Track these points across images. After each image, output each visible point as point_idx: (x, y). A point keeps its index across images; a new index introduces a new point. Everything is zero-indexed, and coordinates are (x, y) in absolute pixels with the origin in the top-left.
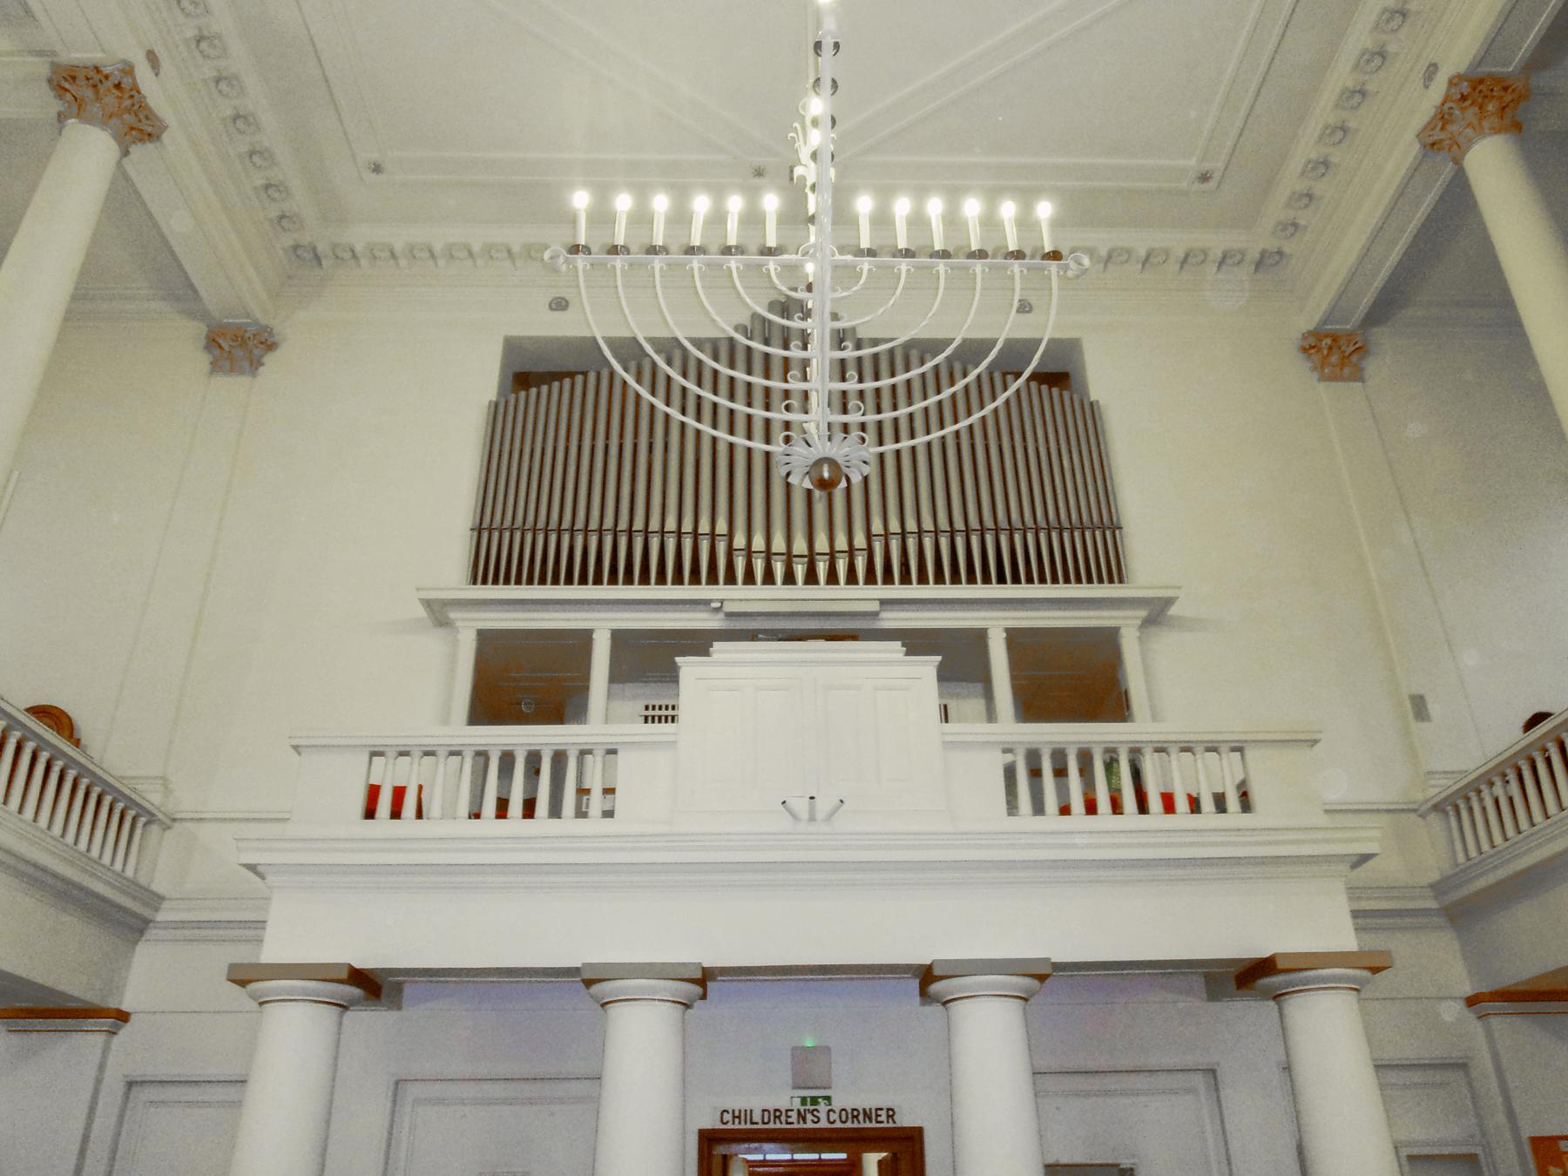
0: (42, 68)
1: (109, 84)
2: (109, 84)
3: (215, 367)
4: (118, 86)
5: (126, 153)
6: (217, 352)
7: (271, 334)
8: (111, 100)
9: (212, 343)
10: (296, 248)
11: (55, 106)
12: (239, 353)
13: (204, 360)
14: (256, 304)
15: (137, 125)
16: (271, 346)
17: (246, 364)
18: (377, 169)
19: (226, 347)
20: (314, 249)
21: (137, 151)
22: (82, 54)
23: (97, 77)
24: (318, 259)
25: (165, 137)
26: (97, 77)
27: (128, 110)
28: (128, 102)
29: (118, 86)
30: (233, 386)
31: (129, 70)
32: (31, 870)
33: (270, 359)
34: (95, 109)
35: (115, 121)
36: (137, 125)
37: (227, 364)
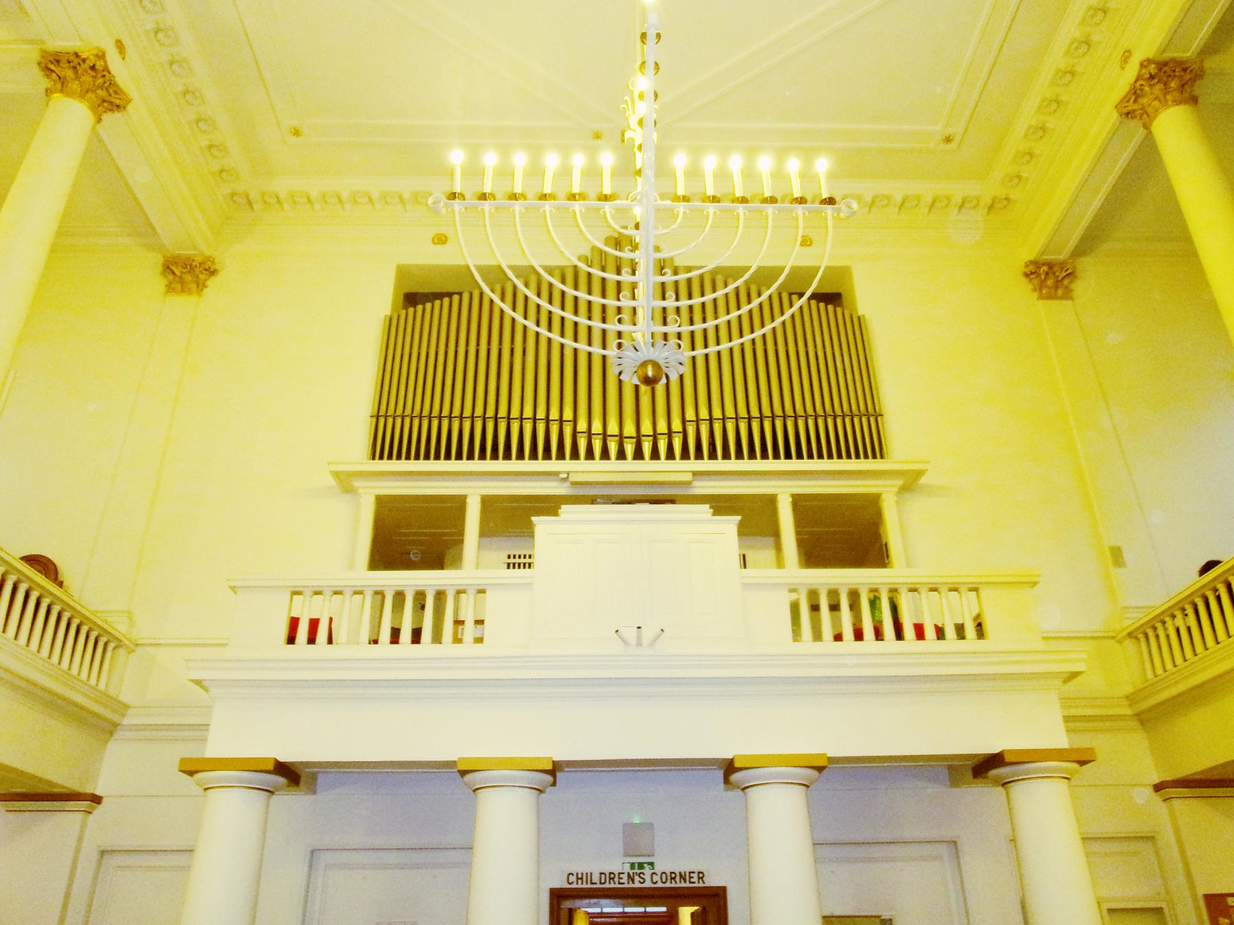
1: (86, 66)
2: (86, 66)
3: (170, 288)
6: (171, 277)
7: (213, 262)
9: (167, 268)
10: (233, 195)
11: (45, 83)
12: (188, 278)
13: (160, 283)
14: (202, 244)
16: (213, 273)
17: (194, 286)
18: (297, 133)
20: (247, 196)
28: (100, 81)
29: (93, 68)
31: (101, 56)
33: (213, 282)
34: (74, 85)
37: (178, 286)
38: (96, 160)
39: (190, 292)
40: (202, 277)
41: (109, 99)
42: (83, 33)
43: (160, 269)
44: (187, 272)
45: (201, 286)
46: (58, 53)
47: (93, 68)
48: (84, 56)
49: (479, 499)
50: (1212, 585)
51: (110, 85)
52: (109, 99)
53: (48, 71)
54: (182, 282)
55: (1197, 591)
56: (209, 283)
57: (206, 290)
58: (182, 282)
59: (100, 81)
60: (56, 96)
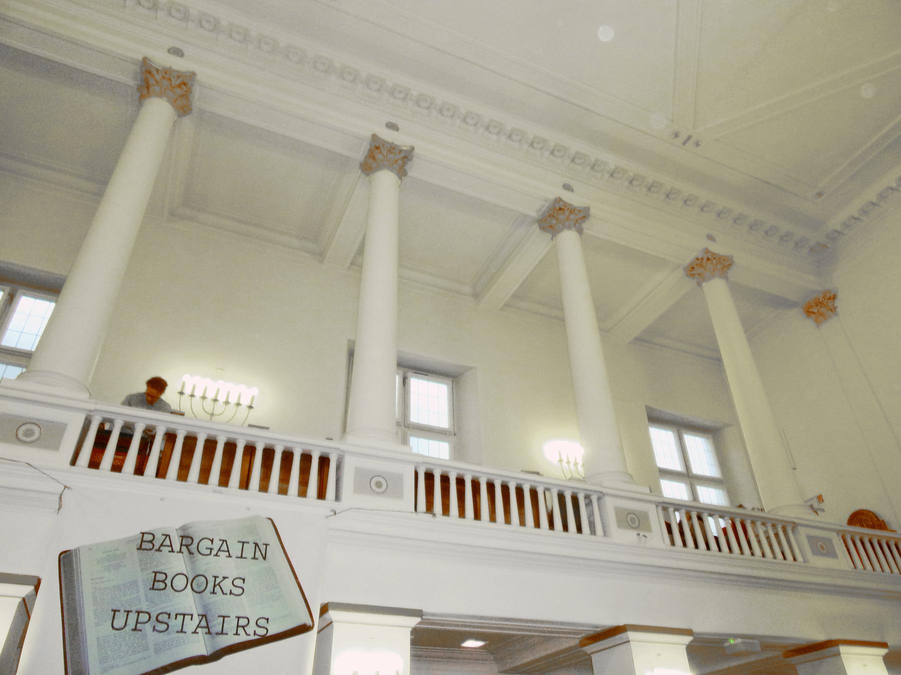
1: (705, 261)
2: (705, 261)
3: (818, 323)
6: (813, 316)
9: (809, 312)
12: (823, 310)
13: (809, 324)
16: (834, 297)
31: (707, 251)
33: (837, 303)
37: (821, 318)
38: (739, 292)
40: (830, 304)
41: (399, 160)
44: (821, 307)
45: (833, 310)
47: (708, 259)
48: (700, 257)
49: (102, 466)
51: (573, 210)
52: (399, 160)
56: (836, 305)
57: (838, 310)
58: (822, 315)
59: (715, 262)
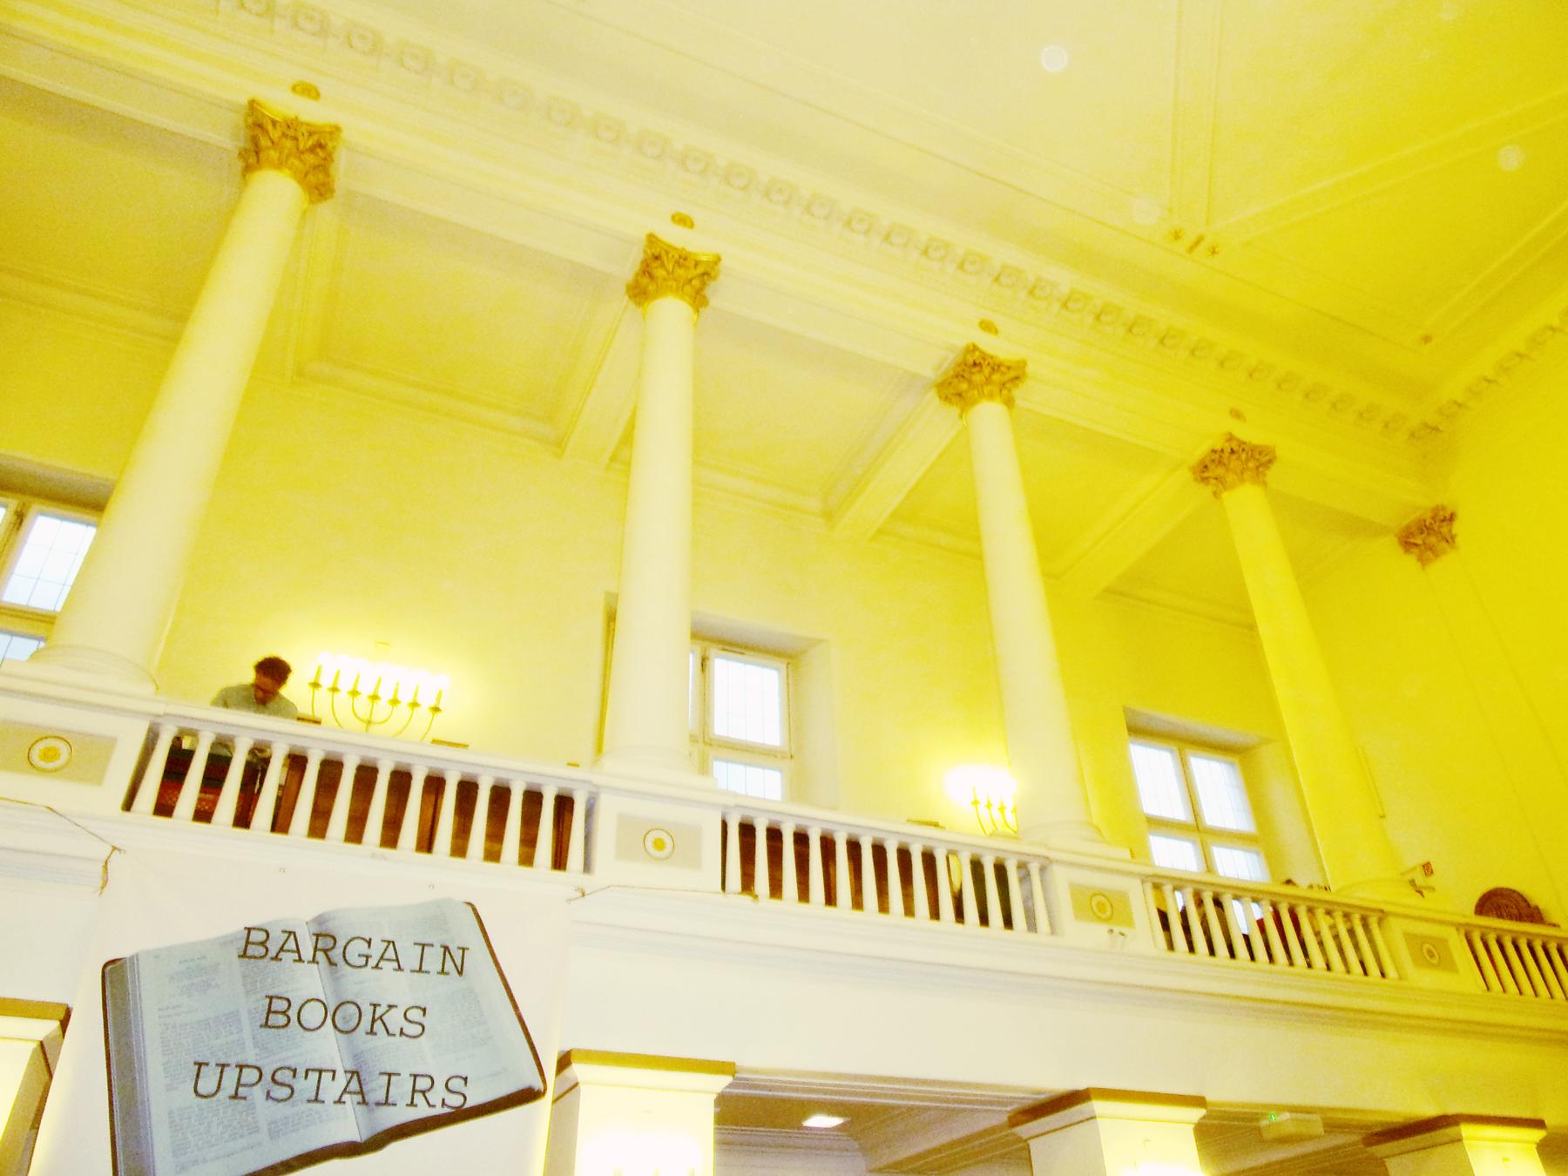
0: (1185, 475)
1: (1226, 455)
2: (1226, 455)
3: (1423, 561)
4: (1232, 451)
5: (1265, 484)
6: (1415, 550)
7: (1443, 508)
8: (1235, 463)
9: (1407, 543)
10: (1412, 435)
11: (1207, 491)
12: (1433, 540)
13: (1410, 561)
14: (1417, 499)
15: (696, 279)
16: (1452, 518)
17: (1444, 544)
18: (1427, 339)
19: (1419, 541)
20: (1426, 425)
21: (1018, 392)
22: (1201, 451)
23: (1216, 456)
24: (1436, 429)
25: (1279, 452)
26: (1216, 456)
27: (1247, 460)
28: (1244, 456)
29: (1232, 451)
30: (1446, 565)
31: (1231, 438)
32: (1449, 1025)
33: (1457, 527)
34: (1230, 478)
35: (1247, 475)
36: (696, 279)
37: (1429, 554)
39: (1445, 552)
40: (1445, 530)
42: (1210, 431)
43: (1400, 550)
44: (1427, 534)
45: (1450, 540)
46: (1202, 461)
48: (1218, 447)
50: (1023, 858)
53: (1205, 480)
54: (1431, 548)
55: (1327, 902)
56: (1455, 531)
57: (1458, 540)
58: (1431, 548)
60: (1225, 495)
